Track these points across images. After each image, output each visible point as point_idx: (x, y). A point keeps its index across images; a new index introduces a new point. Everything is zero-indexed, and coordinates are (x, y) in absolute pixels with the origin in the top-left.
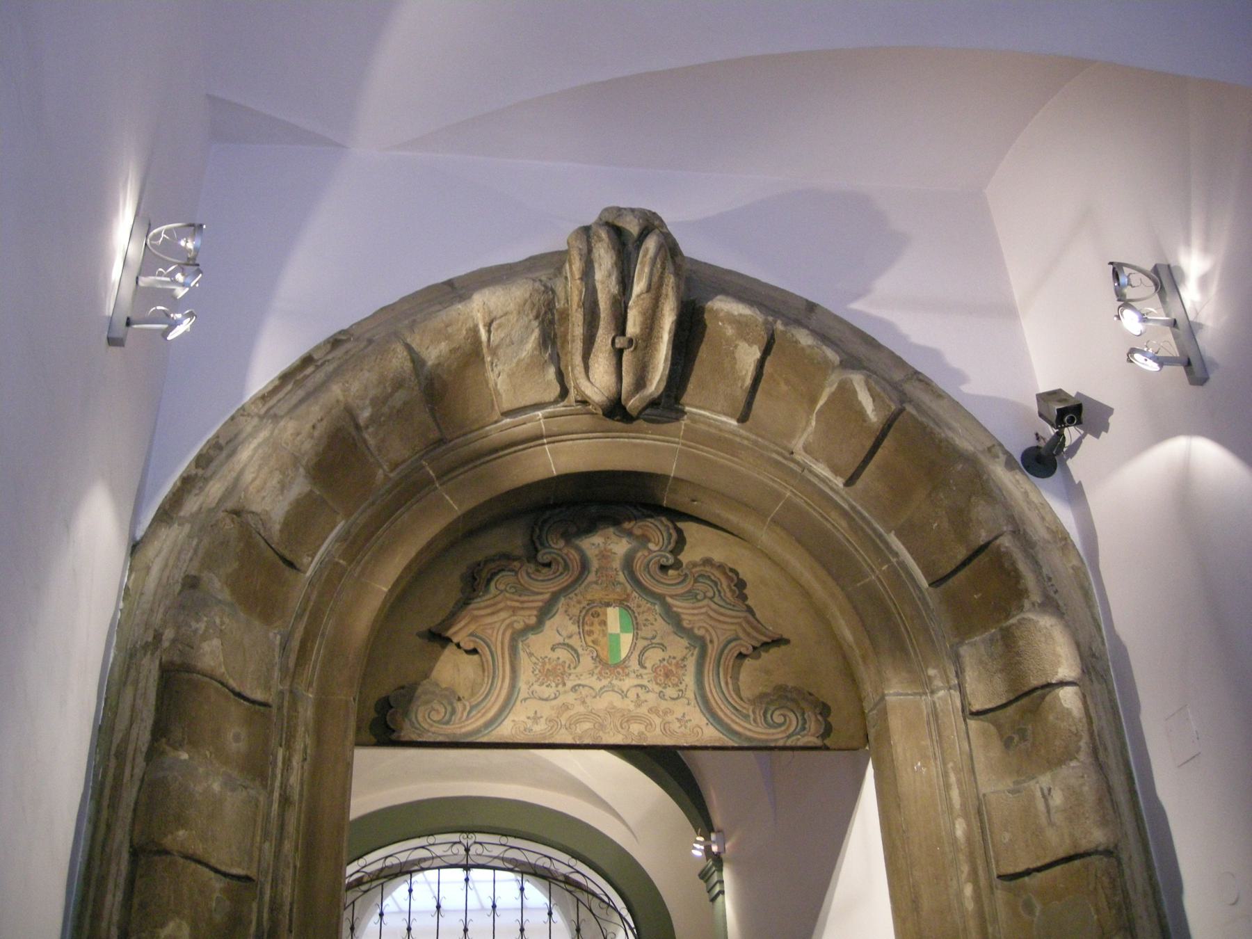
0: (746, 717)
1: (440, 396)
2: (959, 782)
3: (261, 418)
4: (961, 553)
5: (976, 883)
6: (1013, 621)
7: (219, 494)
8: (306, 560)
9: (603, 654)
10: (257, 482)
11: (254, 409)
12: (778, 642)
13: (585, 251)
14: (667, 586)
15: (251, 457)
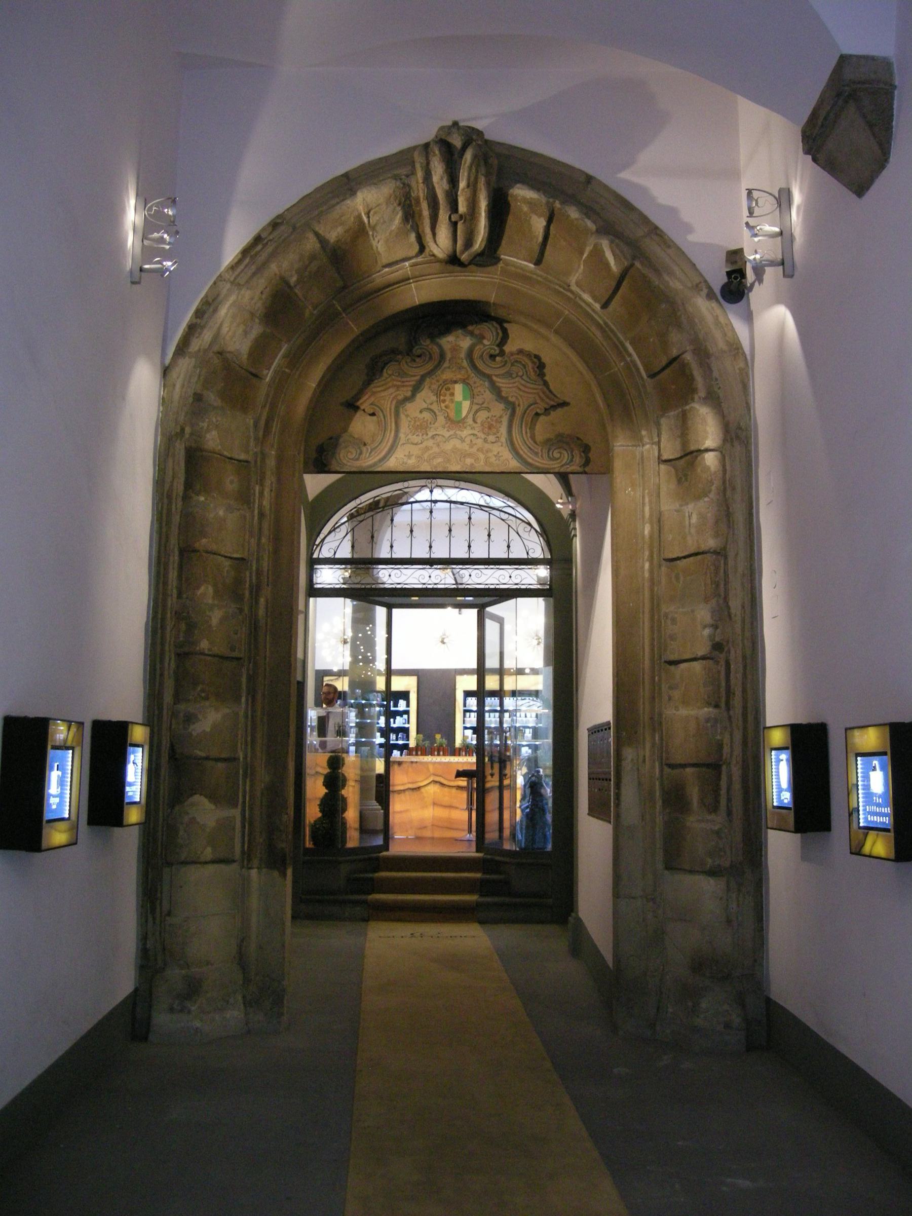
0: (536, 454)
1: (342, 262)
2: (650, 501)
3: (232, 283)
4: (664, 361)
5: (651, 564)
6: (687, 407)
7: (210, 339)
8: (265, 372)
9: (452, 415)
10: (230, 333)
11: (227, 276)
12: (564, 404)
13: (425, 164)
14: (494, 369)
15: (227, 314)
